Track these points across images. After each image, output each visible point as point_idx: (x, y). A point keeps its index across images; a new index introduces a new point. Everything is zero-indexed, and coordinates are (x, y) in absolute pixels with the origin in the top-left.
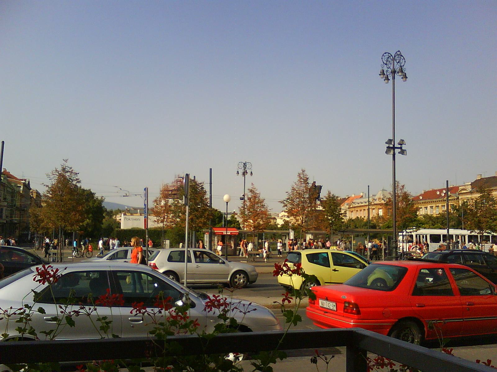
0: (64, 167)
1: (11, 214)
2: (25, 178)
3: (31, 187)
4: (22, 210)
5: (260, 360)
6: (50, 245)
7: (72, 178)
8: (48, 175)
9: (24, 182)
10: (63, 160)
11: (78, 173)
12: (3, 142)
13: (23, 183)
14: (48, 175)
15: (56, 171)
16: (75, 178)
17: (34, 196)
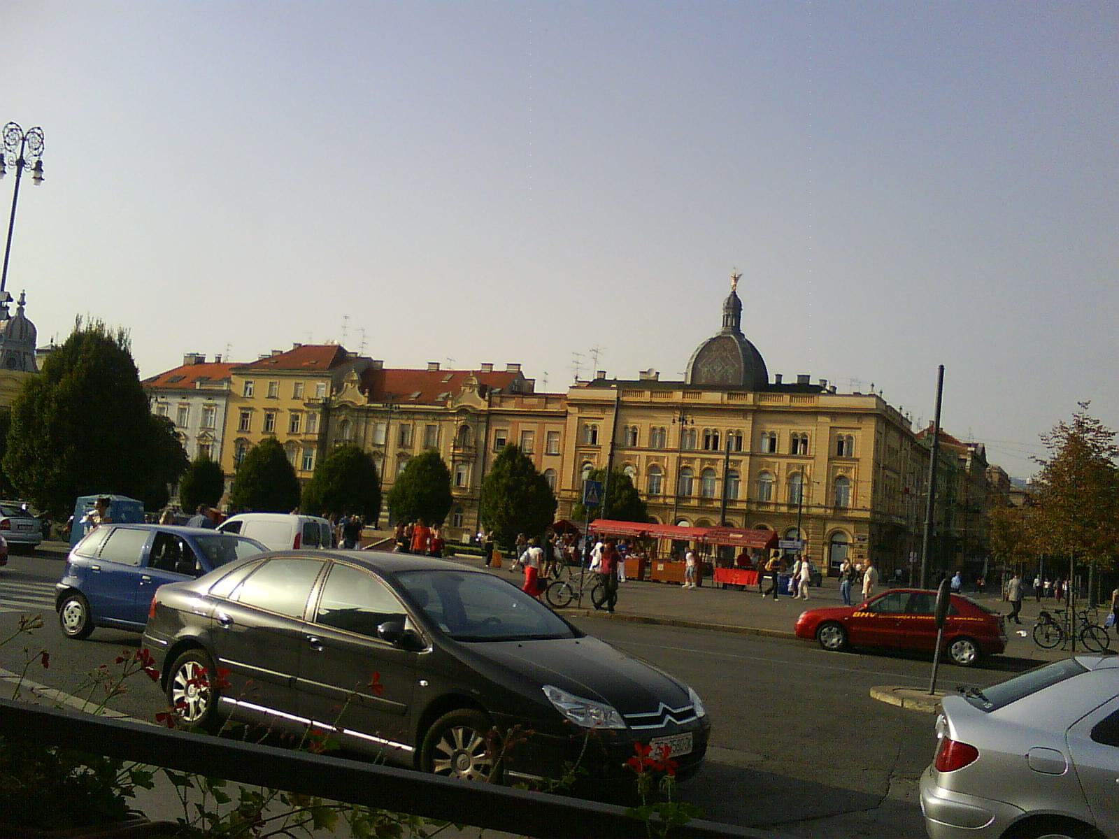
0: (1081, 420)
1: (948, 519)
2: (975, 442)
3: (987, 460)
4: (971, 511)
5: (201, 776)
6: (855, 566)
7: (1098, 445)
8: (1044, 439)
9: (973, 449)
10: (1079, 403)
11: (1114, 434)
12: (942, 368)
13: (972, 452)
14: (1044, 438)
15: (1062, 427)
16: (1106, 443)
17: (996, 477)
